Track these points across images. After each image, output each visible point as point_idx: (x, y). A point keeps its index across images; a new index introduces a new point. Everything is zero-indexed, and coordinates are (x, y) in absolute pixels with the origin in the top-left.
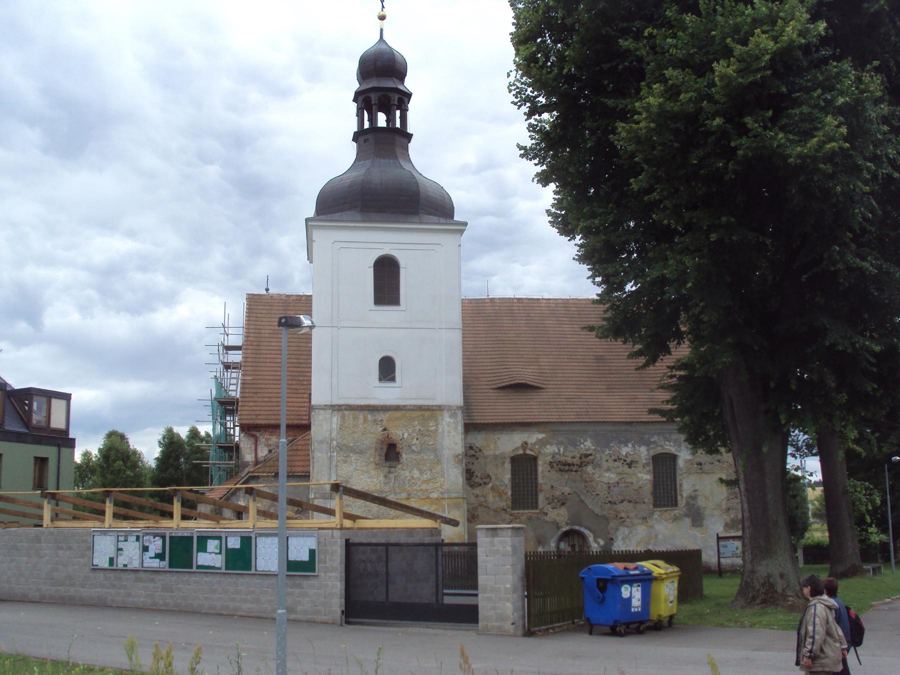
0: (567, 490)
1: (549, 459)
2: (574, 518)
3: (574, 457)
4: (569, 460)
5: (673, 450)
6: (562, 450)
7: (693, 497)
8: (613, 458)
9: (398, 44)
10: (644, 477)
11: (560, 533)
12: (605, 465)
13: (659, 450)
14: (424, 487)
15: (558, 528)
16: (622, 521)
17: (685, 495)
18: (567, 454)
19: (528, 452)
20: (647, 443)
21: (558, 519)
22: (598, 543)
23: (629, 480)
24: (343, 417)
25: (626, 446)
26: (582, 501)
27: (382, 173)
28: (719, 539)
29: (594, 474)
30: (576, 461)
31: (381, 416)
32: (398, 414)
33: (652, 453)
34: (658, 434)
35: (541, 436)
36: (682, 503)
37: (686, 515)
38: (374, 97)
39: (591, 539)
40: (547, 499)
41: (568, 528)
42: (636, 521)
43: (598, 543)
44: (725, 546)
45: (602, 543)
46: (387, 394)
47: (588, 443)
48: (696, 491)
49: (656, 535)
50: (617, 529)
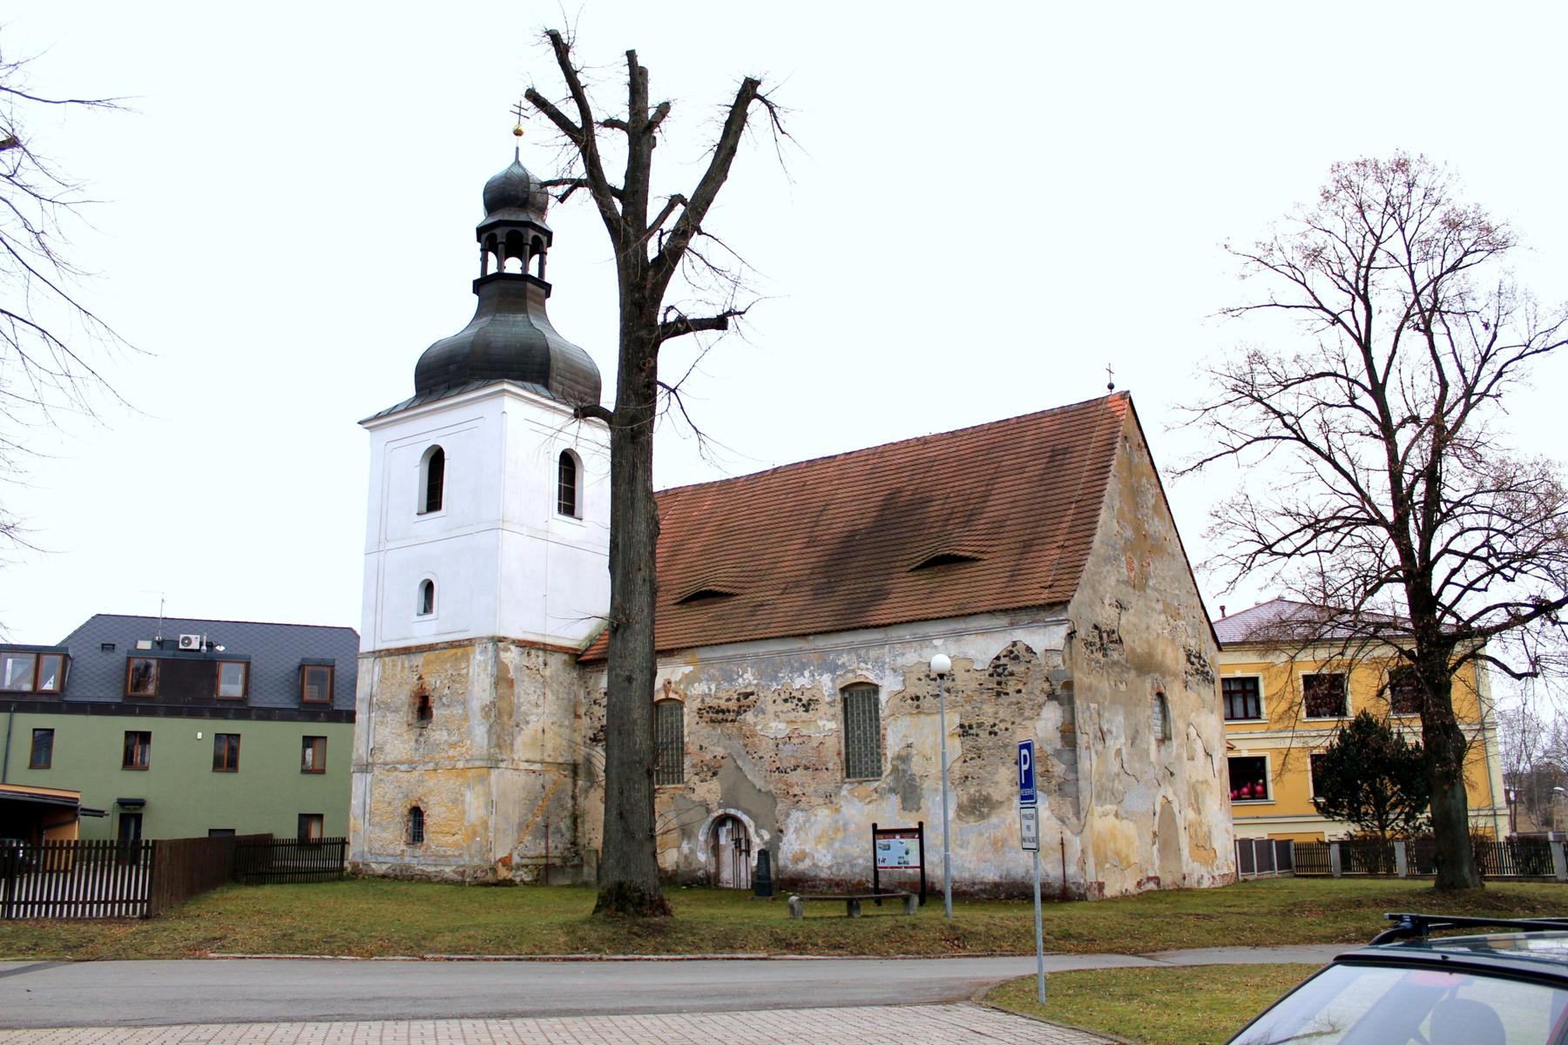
0: (720, 751)
1: (697, 704)
2: (729, 799)
3: (729, 700)
4: (724, 705)
5: (872, 677)
6: (713, 687)
7: (904, 758)
10: (827, 726)
12: (771, 708)
14: (451, 752)
15: (708, 811)
16: (796, 801)
17: (890, 754)
19: (671, 695)
20: (833, 669)
21: (708, 797)
22: (762, 838)
23: (805, 732)
24: (384, 665)
25: (802, 674)
27: (509, 329)
28: (877, 832)
30: (733, 705)
31: (419, 660)
32: (432, 655)
33: (841, 683)
34: (849, 652)
35: (688, 669)
36: (887, 767)
37: (892, 790)
38: (501, 234)
39: (751, 830)
40: (694, 766)
41: (721, 812)
42: (815, 800)
43: (762, 838)
44: (888, 848)
45: (767, 837)
46: (425, 631)
47: (749, 676)
48: (909, 746)
49: (845, 825)
50: (788, 815)
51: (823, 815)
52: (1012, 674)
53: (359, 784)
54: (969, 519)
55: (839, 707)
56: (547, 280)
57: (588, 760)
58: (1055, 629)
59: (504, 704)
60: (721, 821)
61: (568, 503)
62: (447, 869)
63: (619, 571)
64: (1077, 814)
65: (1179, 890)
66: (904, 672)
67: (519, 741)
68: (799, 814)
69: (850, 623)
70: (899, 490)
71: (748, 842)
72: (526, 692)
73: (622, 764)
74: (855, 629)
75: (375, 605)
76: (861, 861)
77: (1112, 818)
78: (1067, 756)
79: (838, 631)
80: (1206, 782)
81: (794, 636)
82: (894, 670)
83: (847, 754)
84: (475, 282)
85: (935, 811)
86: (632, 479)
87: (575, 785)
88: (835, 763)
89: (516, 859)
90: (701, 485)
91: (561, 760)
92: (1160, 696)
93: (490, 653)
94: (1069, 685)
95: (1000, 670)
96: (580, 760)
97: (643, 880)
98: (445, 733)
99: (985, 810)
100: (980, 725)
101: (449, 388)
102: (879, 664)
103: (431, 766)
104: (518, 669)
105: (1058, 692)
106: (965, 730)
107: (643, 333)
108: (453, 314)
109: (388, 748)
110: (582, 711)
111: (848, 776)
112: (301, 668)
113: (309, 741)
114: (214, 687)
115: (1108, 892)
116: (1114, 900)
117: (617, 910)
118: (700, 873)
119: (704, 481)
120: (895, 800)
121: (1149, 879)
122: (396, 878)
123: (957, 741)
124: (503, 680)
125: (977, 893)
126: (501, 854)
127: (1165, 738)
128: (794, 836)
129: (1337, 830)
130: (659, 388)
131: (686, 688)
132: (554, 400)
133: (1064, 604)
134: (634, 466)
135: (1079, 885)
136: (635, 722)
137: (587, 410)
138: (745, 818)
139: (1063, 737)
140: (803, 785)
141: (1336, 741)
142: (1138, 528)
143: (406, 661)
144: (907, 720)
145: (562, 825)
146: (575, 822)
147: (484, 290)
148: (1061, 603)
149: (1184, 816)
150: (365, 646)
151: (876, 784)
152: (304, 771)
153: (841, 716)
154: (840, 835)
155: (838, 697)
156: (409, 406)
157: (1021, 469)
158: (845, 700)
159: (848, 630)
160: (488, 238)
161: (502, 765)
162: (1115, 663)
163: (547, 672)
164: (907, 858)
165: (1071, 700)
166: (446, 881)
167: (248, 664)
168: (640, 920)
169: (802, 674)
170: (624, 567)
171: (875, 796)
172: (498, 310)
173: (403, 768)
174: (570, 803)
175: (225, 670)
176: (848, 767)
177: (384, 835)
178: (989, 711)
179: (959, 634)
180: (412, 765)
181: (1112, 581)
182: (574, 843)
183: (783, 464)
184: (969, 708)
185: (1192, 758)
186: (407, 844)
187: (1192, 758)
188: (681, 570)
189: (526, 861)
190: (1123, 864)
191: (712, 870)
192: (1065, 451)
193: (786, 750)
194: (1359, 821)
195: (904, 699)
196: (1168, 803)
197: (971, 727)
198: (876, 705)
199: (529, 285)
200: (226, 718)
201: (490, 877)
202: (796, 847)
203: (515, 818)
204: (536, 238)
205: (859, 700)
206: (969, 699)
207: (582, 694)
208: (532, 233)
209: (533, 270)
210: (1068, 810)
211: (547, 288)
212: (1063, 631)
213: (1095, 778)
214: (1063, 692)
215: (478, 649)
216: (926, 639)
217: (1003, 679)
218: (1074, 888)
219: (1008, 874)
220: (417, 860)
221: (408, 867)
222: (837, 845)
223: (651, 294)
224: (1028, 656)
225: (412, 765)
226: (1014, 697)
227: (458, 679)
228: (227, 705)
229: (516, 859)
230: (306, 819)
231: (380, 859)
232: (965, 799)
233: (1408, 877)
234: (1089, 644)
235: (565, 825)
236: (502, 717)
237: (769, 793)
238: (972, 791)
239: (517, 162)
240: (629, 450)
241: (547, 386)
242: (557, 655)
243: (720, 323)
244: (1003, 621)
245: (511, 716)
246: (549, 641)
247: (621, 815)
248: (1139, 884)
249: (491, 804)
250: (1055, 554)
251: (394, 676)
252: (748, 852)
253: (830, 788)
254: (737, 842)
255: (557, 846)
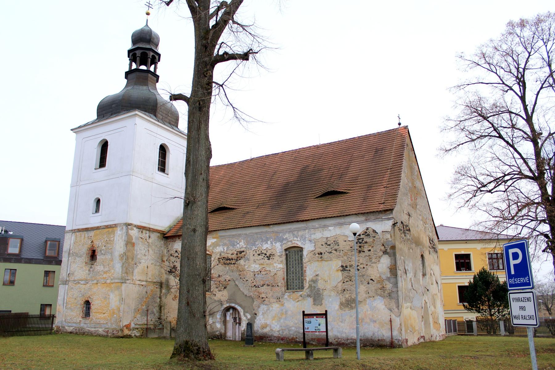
3: (232, 254)
4: (230, 256)
5: (300, 244)
6: (225, 249)
7: (314, 281)
8: (258, 253)
9: (155, 28)
10: (278, 266)
11: (223, 308)
12: (252, 258)
13: (290, 245)
16: (263, 300)
17: (308, 279)
18: (228, 252)
20: (281, 240)
22: (246, 317)
23: (268, 269)
25: (267, 243)
26: (236, 285)
27: (140, 92)
28: (304, 315)
29: (245, 265)
30: (234, 256)
31: (92, 234)
32: (98, 232)
34: (289, 232)
36: (306, 285)
37: (309, 296)
38: (138, 53)
39: (242, 314)
41: (228, 305)
42: (272, 300)
43: (246, 317)
45: (249, 317)
46: (96, 221)
47: (242, 244)
49: (286, 312)
50: (259, 307)
51: (276, 307)
52: (366, 243)
53: (62, 290)
54: (341, 176)
55: (284, 257)
56: (157, 73)
57: (167, 281)
58: (387, 222)
59: (129, 254)
60: (228, 309)
61: (162, 167)
62: (100, 330)
63: (190, 175)
64: (398, 307)
65: (431, 341)
66: (314, 242)
67: (136, 271)
68: (265, 306)
69: (290, 220)
70: (308, 166)
71: (240, 319)
72: (140, 249)
73: (189, 276)
74: (292, 222)
75: (73, 209)
76: (293, 328)
77: (409, 309)
78: (393, 280)
79: (284, 223)
80: (436, 294)
81: (263, 225)
82: (310, 241)
83: (287, 279)
84: (126, 73)
85: (332, 304)
86: (199, 128)
87: (161, 292)
88: (282, 283)
89: (133, 325)
90: (219, 166)
91: (155, 281)
92: (422, 256)
93: (124, 230)
94: (393, 247)
95: (360, 241)
96: (164, 281)
97: (198, 339)
98: (102, 267)
99: (353, 305)
100: (351, 266)
101: (112, 115)
102: (303, 238)
103: (95, 281)
104: (137, 238)
105: (388, 250)
106: (344, 268)
107: (207, 59)
108: (116, 85)
109: (76, 273)
110: (165, 259)
111: (288, 289)
112: (46, 242)
113: (47, 273)
114: (6, 249)
115: (410, 343)
116: (411, 346)
117: (185, 356)
118: (217, 333)
119: (221, 164)
120: (310, 300)
121: (422, 337)
122: (76, 333)
123: (340, 273)
124: (129, 243)
125: (349, 344)
126: (126, 323)
127: (424, 275)
128: (262, 317)
129: (472, 316)
130: (214, 85)
131: (213, 249)
132: (158, 121)
133: (391, 210)
134: (200, 122)
135: (399, 340)
136: (197, 254)
137: (172, 120)
138: (239, 308)
139: (390, 271)
140: (266, 293)
141: (472, 280)
142: (413, 184)
143: (86, 234)
144: (316, 264)
145: (154, 310)
146: (160, 307)
147: (129, 76)
148: (390, 210)
149: (431, 309)
150: (67, 229)
151: (301, 293)
152: (44, 286)
153: (285, 262)
154: (284, 316)
155: (284, 253)
156: (93, 123)
157: (363, 157)
158: (287, 255)
159: (289, 222)
160: (132, 55)
161: (128, 282)
162: (409, 239)
163: (150, 241)
164: (319, 327)
165: (395, 254)
166: (100, 335)
167: (22, 240)
168: (197, 363)
169: (267, 243)
170: (193, 173)
171: (300, 298)
172: (136, 84)
173: (82, 282)
174: (159, 300)
175: (11, 241)
176: (287, 285)
177: (72, 313)
178: (356, 259)
179: (341, 224)
180: (86, 282)
181: (406, 203)
182: (159, 319)
183: (255, 157)
184: (345, 258)
185: (432, 284)
186: (83, 318)
187: (432, 284)
188: (214, 197)
189: (137, 326)
190: (413, 331)
191: (223, 332)
192: (382, 149)
193: (259, 277)
194: (479, 312)
195: (315, 254)
196: (430, 304)
197: (346, 267)
198: (301, 256)
199: (150, 75)
200: (11, 262)
201: (120, 334)
202: (263, 321)
203: (133, 306)
204: (153, 56)
205: (293, 255)
206: (346, 254)
207: (165, 251)
208: (152, 54)
209: (152, 69)
210: (393, 305)
211: (157, 77)
212: (391, 223)
213: (404, 291)
214: (390, 251)
215: (119, 229)
216: (325, 226)
217: (362, 245)
218: (396, 342)
219: (364, 335)
220: (87, 325)
221: (82, 328)
222: (282, 321)
223: (211, 43)
224: (374, 234)
225: (86, 282)
226: (367, 253)
227: (109, 242)
228: (11, 257)
229: (133, 325)
230: (44, 307)
231: (70, 325)
232: (344, 300)
233: (505, 336)
234: (400, 230)
235: (156, 310)
236: (129, 260)
237: (250, 297)
238: (347, 296)
239: (147, 25)
240: (198, 114)
241: (155, 116)
242: (155, 233)
243: (245, 57)
244: (362, 218)
245: (133, 259)
246: (152, 227)
247: (188, 304)
248: (418, 339)
249: (122, 300)
250: (383, 190)
251: (81, 241)
252: (240, 324)
253: (279, 295)
254: (235, 319)
255: (152, 319)
